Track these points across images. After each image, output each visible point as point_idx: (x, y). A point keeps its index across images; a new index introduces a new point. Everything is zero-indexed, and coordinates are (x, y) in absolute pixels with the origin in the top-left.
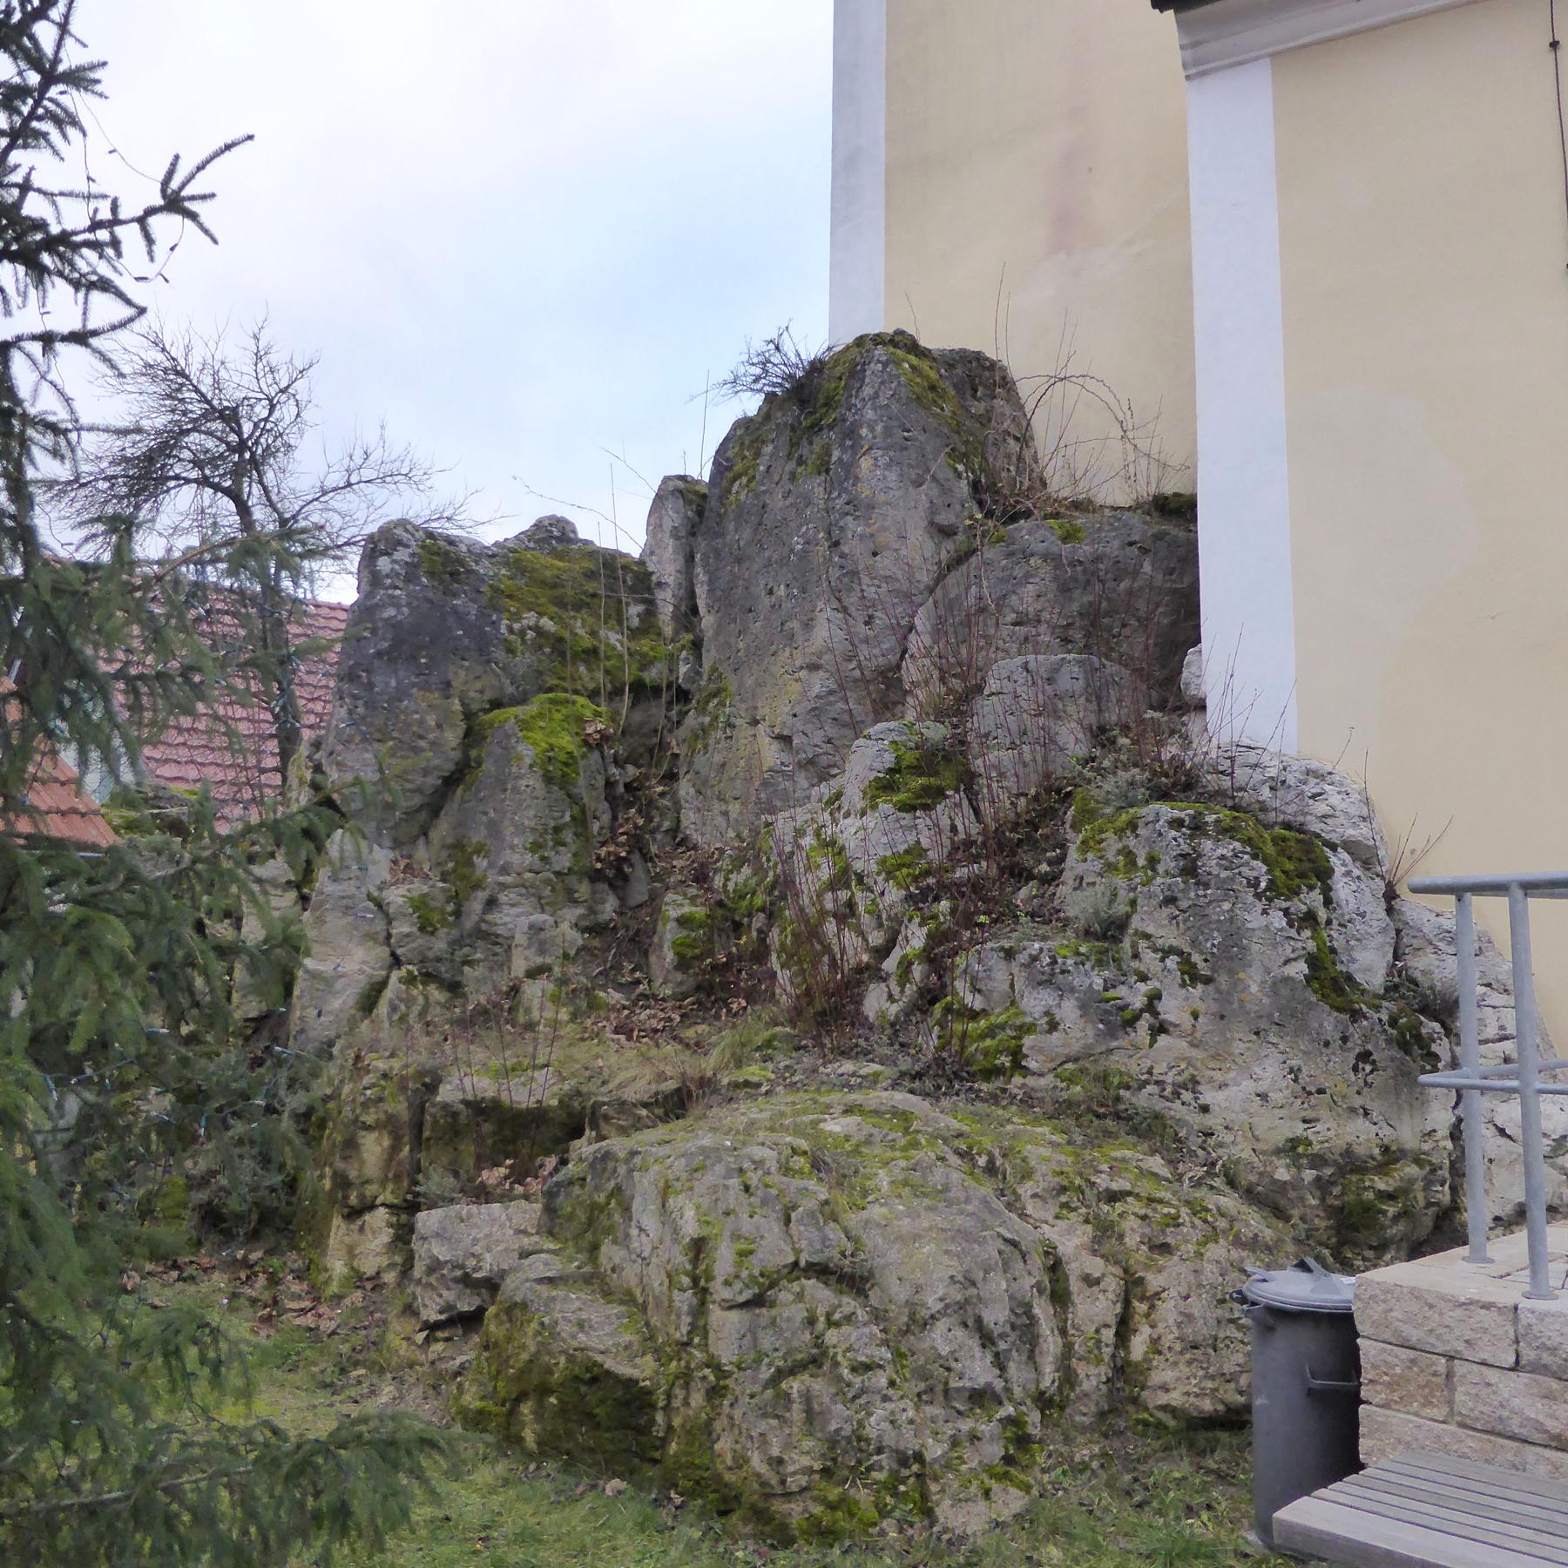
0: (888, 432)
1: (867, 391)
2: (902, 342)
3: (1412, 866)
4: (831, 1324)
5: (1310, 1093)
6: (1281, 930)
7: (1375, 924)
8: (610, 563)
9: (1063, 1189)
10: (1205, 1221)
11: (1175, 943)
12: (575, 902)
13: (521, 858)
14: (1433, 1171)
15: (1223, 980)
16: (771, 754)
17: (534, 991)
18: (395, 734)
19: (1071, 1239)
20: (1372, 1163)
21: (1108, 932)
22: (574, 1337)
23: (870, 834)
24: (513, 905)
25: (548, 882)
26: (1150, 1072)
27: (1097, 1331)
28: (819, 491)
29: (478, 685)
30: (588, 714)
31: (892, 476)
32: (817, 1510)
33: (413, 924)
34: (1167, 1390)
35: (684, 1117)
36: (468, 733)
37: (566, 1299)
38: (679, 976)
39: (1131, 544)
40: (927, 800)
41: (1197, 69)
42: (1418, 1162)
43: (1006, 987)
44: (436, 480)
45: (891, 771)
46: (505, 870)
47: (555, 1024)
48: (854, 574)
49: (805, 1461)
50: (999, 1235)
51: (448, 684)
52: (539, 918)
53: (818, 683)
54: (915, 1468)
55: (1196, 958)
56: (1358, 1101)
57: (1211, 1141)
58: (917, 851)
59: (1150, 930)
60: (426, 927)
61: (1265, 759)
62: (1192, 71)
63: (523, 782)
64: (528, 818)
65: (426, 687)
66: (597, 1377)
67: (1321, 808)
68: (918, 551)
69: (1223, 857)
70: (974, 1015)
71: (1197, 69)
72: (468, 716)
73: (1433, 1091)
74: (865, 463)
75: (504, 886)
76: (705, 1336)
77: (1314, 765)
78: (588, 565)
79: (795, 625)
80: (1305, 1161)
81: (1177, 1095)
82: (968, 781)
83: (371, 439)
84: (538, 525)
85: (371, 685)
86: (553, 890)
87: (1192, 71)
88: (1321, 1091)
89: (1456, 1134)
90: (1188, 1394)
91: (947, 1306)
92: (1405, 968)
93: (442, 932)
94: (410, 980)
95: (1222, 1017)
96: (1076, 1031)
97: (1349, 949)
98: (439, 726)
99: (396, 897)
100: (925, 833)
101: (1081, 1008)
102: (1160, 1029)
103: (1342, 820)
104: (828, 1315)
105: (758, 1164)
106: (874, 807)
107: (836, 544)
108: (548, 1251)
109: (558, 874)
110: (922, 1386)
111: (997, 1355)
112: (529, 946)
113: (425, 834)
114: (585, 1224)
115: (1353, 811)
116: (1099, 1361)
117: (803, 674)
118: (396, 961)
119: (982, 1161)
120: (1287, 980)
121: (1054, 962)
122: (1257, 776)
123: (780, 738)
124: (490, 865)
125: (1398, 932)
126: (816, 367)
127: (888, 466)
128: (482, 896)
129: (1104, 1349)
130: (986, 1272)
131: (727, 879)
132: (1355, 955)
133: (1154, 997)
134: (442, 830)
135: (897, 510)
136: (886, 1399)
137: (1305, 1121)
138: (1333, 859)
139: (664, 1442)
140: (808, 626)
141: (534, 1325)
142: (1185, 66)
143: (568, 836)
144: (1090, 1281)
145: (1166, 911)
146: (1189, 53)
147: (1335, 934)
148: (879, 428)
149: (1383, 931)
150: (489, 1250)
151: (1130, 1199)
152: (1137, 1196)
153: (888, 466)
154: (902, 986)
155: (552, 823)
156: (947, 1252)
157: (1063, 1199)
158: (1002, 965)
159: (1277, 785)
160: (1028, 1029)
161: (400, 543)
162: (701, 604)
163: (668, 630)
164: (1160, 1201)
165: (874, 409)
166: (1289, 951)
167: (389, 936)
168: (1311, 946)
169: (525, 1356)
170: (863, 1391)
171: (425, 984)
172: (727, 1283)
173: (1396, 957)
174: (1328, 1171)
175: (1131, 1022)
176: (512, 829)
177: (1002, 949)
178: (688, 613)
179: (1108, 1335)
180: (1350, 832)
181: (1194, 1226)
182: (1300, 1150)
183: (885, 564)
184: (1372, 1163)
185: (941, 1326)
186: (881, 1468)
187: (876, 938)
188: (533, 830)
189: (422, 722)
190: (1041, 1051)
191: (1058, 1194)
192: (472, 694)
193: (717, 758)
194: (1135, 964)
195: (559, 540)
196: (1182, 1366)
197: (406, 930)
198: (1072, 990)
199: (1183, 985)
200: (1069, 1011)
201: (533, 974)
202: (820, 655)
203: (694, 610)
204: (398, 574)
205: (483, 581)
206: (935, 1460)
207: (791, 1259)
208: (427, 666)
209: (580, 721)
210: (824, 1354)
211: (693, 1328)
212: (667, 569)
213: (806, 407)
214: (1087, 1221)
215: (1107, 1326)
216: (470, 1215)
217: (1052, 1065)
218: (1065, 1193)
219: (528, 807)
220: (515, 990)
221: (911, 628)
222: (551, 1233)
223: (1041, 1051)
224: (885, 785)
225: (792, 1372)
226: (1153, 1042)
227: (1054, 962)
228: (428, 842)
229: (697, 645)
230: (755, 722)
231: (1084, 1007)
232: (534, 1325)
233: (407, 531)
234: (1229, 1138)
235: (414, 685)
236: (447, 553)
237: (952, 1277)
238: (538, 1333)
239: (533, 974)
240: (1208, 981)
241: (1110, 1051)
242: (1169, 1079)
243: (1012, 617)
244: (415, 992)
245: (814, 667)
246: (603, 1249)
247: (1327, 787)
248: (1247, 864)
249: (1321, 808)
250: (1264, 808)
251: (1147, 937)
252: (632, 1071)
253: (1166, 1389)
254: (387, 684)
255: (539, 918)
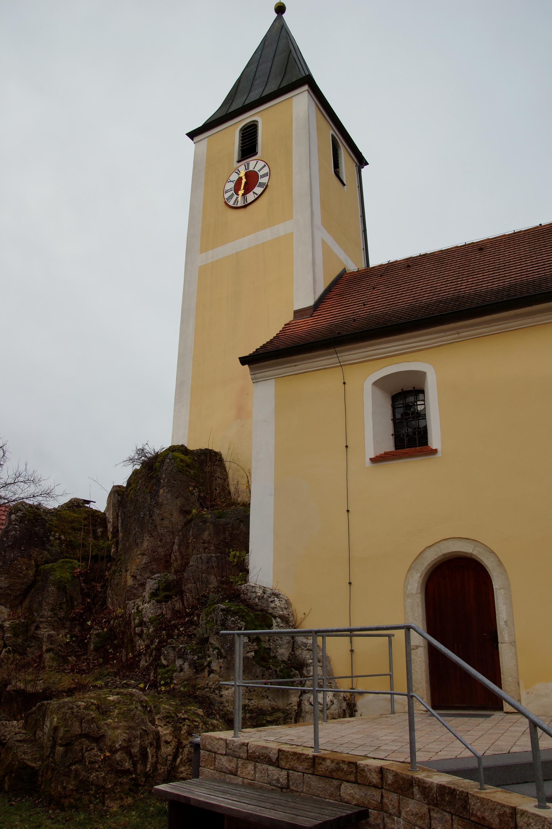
0: (169, 481)
1: (164, 468)
2: (182, 449)
3: (301, 622)
4: (87, 751)
5: (251, 691)
6: (246, 643)
7: (285, 641)
8: (95, 514)
9: (167, 717)
10: (206, 727)
11: (217, 646)
12: (65, 628)
13: (47, 613)
14: (288, 715)
15: (229, 658)
16: (130, 582)
17: (47, 656)
18: (12, 572)
19: (165, 731)
20: (268, 713)
21: (204, 641)
22: (21, 756)
23: (149, 609)
24: (44, 628)
25: (56, 621)
26: (208, 685)
27: (167, 757)
28: (149, 498)
29: (41, 556)
30: (76, 566)
31: (169, 496)
32: (72, 800)
33: (12, 634)
34: (182, 773)
35: (71, 696)
36: (36, 571)
37: (23, 746)
38: (95, 653)
39: (238, 519)
40: (167, 598)
41: (255, 381)
42: (283, 713)
43: (173, 658)
44: (42, 483)
45: (156, 590)
46: (42, 617)
47: (50, 667)
48: (156, 526)
49: (71, 787)
50: (142, 728)
51: (31, 556)
52: (52, 632)
53: (145, 560)
54: (102, 790)
55: (222, 651)
56: (265, 694)
57: (222, 705)
58: (162, 615)
59: (212, 642)
60: (16, 635)
61: (257, 590)
62: (254, 381)
63: (50, 589)
64: (51, 600)
65: (23, 557)
66: (25, 767)
67: (273, 605)
68: (177, 519)
69: (233, 621)
70: (164, 666)
71: (255, 381)
72: (37, 566)
73: (291, 691)
74: (161, 491)
75: (42, 622)
76: (54, 755)
77: (276, 591)
78: (85, 515)
79: (138, 540)
80: (247, 712)
81: (214, 691)
82: (181, 593)
83: (22, 468)
84: (71, 501)
85: (5, 556)
86: (58, 624)
87: (254, 381)
88: (254, 691)
89: (300, 704)
90: (187, 774)
91: (122, 747)
92: (294, 654)
93: (21, 637)
94: (9, 652)
95: (228, 668)
96: (187, 670)
97: (276, 648)
98: (27, 569)
99: (7, 624)
100: (166, 610)
101: (189, 665)
102: (211, 672)
103: (279, 609)
104: (87, 748)
105: (78, 706)
106: (150, 601)
107: (151, 516)
108: (23, 733)
109: (59, 618)
110: (110, 769)
111: (133, 761)
112: (47, 642)
113: (22, 604)
114: (33, 726)
115: (282, 606)
116: (166, 765)
117: (140, 556)
118: (5, 646)
119: (149, 709)
120: (248, 657)
121: (185, 650)
122: (254, 595)
123: (132, 576)
124: (38, 615)
125: (293, 643)
126: (157, 456)
127: (168, 492)
128: (35, 625)
129: (168, 762)
130: (135, 738)
131: (114, 622)
132: (279, 650)
133: (210, 662)
134: (26, 603)
135: (169, 507)
136: (97, 771)
137: (249, 700)
138: (274, 621)
139: (41, 785)
140: (142, 542)
141: (12, 753)
142: (252, 380)
143: (64, 606)
144: (167, 742)
145: (216, 636)
146: (253, 376)
147: (271, 644)
148: (166, 480)
149: (288, 643)
150: (9, 734)
151: (187, 721)
152: (189, 720)
153: (168, 492)
154: (149, 657)
155: (59, 602)
156: (125, 733)
157: (168, 720)
158: (173, 652)
159: (261, 598)
160: (175, 671)
161: (20, 510)
162: (119, 529)
163: (110, 537)
164: (195, 721)
165: (165, 474)
166: (248, 649)
167: (4, 637)
168: (256, 647)
169: (8, 762)
170: (91, 768)
171: (14, 653)
172: (61, 739)
173: (293, 650)
174: (254, 715)
175: (203, 670)
176: (45, 604)
177: (172, 647)
178: (115, 532)
179: (170, 758)
180: (281, 613)
181: (202, 728)
182: (246, 708)
183: (166, 523)
184: (268, 713)
185: (119, 753)
186: (92, 790)
187: (147, 642)
188: (52, 604)
189: (21, 568)
190: (178, 677)
191: (166, 718)
192: (39, 559)
193: (116, 582)
194: (208, 652)
195: (77, 506)
196: (187, 767)
197: (9, 635)
198: (188, 659)
199: (218, 659)
200: (186, 666)
201: (48, 651)
202: (145, 551)
203: (118, 531)
204: (17, 520)
205: (47, 522)
206: (108, 788)
207: (80, 733)
208: (24, 550)
209: (74, 568)
210: (83, 759)
211: (51, 752)
212: (110, 517)
213: (153, 469)
214: (172, 727)
215: (170, 755)
216: (6, 724)
217: (180, 682)
218: (168, 719)
219: (51, 597)
220: (41, 656)
221: (174, 543)
222: (25, 729)
223: (178, 677)
224: (154, 595)
225: (74, 764)
226: (209, 675)
227: (185, 650)
228: (22, 607)
229: (117, 543)
230: (127, 571)
231: (190, 665)
232: (12, 753)
233: (22, 505)
234: (227, 705)
235: (19, 556)
236: (36, 512)
237: (124, 739)
238: (13, 755)
239: (48, 651)
240: (225, 657)
241: (197, 678)
242: (213, 687)
243: (201, 541)
244: (10, 656)
245: (143, 554)
246: (37, 732)
247: (276, 599)
248: (239, 623)
249: (273, 605)
250: (257, 605)
251: (211, 644)
252: (66, 681)
253: (182, 772)
254: (10, 556)
255: (52, 632)
